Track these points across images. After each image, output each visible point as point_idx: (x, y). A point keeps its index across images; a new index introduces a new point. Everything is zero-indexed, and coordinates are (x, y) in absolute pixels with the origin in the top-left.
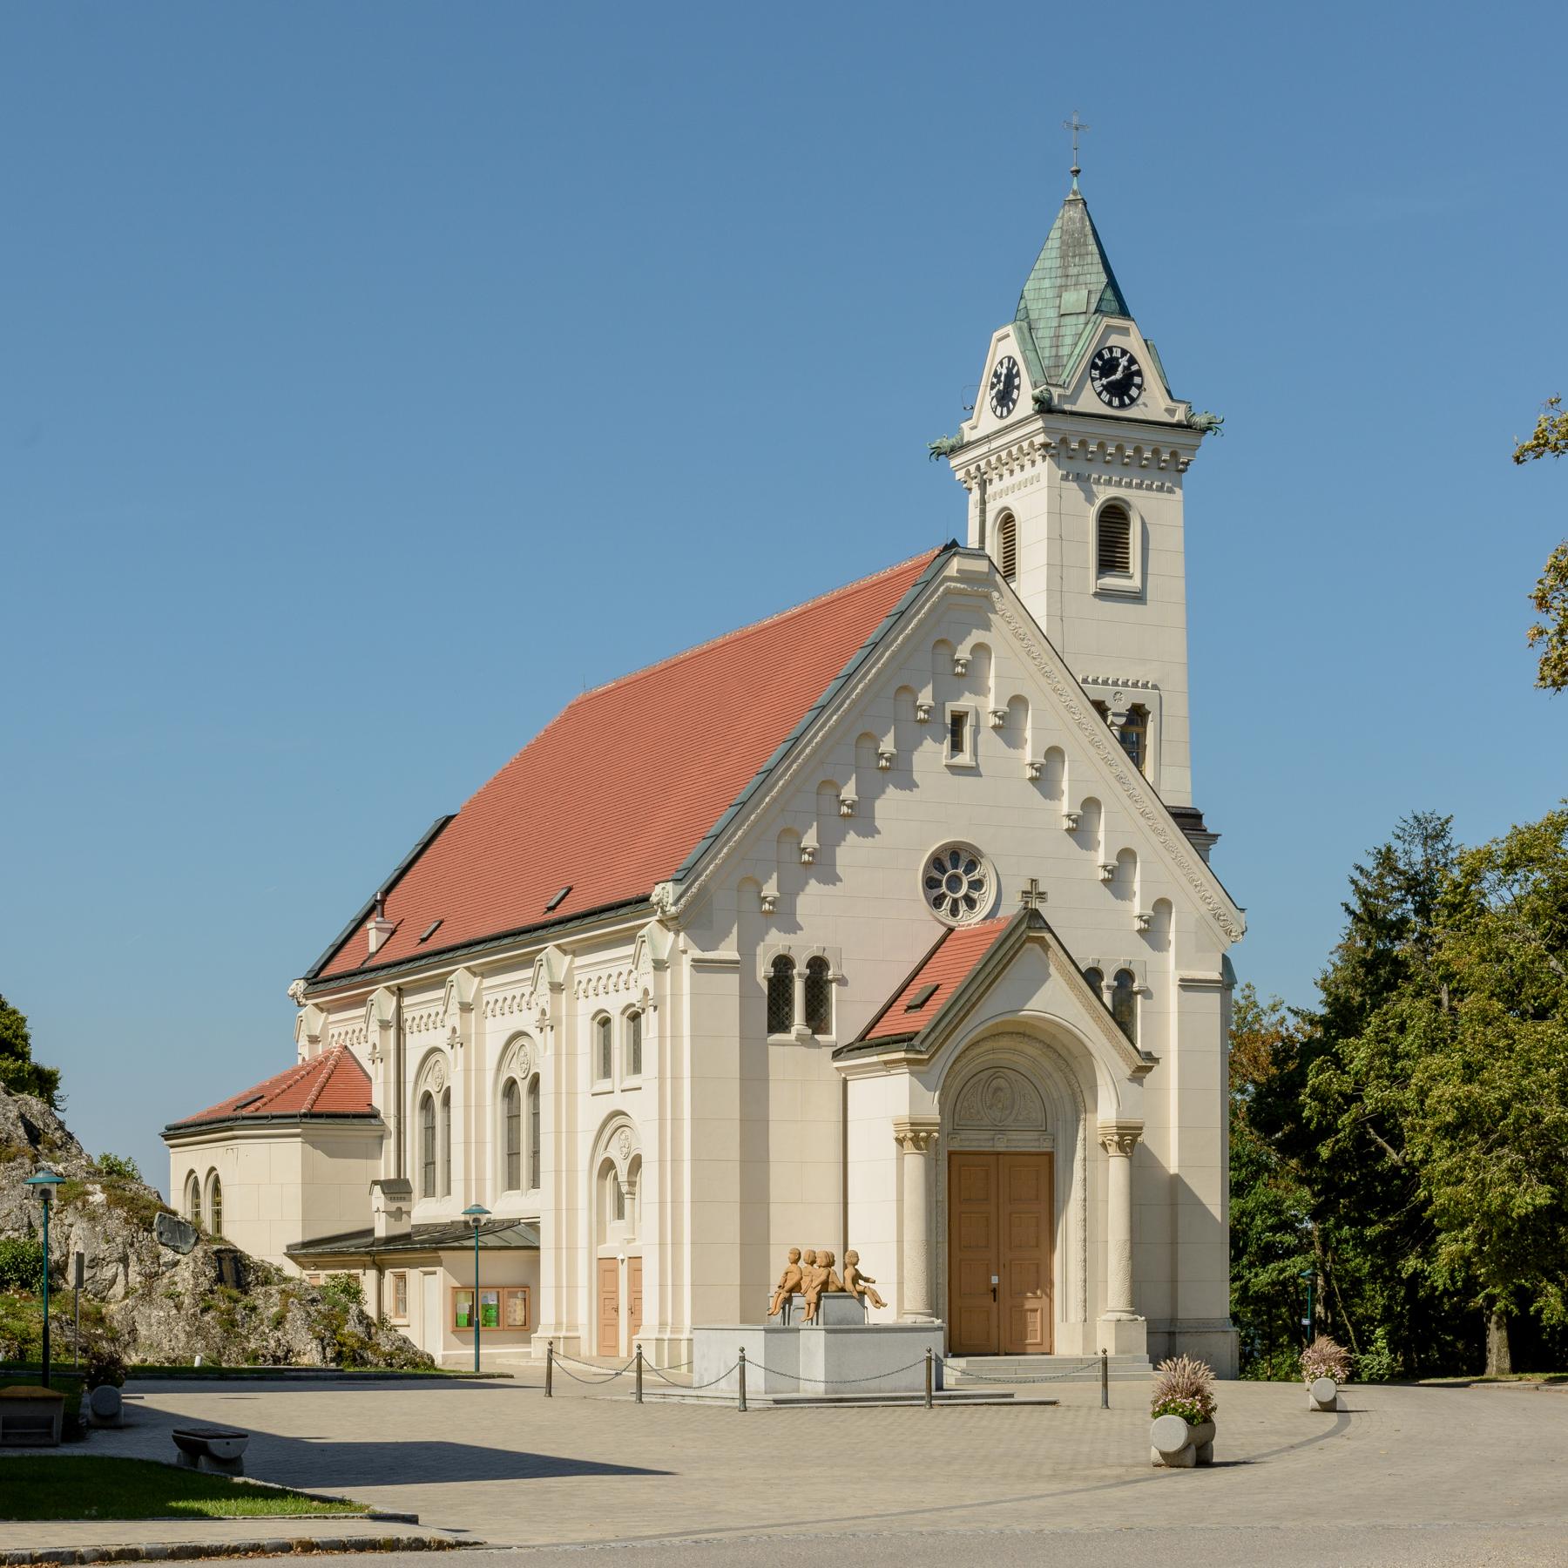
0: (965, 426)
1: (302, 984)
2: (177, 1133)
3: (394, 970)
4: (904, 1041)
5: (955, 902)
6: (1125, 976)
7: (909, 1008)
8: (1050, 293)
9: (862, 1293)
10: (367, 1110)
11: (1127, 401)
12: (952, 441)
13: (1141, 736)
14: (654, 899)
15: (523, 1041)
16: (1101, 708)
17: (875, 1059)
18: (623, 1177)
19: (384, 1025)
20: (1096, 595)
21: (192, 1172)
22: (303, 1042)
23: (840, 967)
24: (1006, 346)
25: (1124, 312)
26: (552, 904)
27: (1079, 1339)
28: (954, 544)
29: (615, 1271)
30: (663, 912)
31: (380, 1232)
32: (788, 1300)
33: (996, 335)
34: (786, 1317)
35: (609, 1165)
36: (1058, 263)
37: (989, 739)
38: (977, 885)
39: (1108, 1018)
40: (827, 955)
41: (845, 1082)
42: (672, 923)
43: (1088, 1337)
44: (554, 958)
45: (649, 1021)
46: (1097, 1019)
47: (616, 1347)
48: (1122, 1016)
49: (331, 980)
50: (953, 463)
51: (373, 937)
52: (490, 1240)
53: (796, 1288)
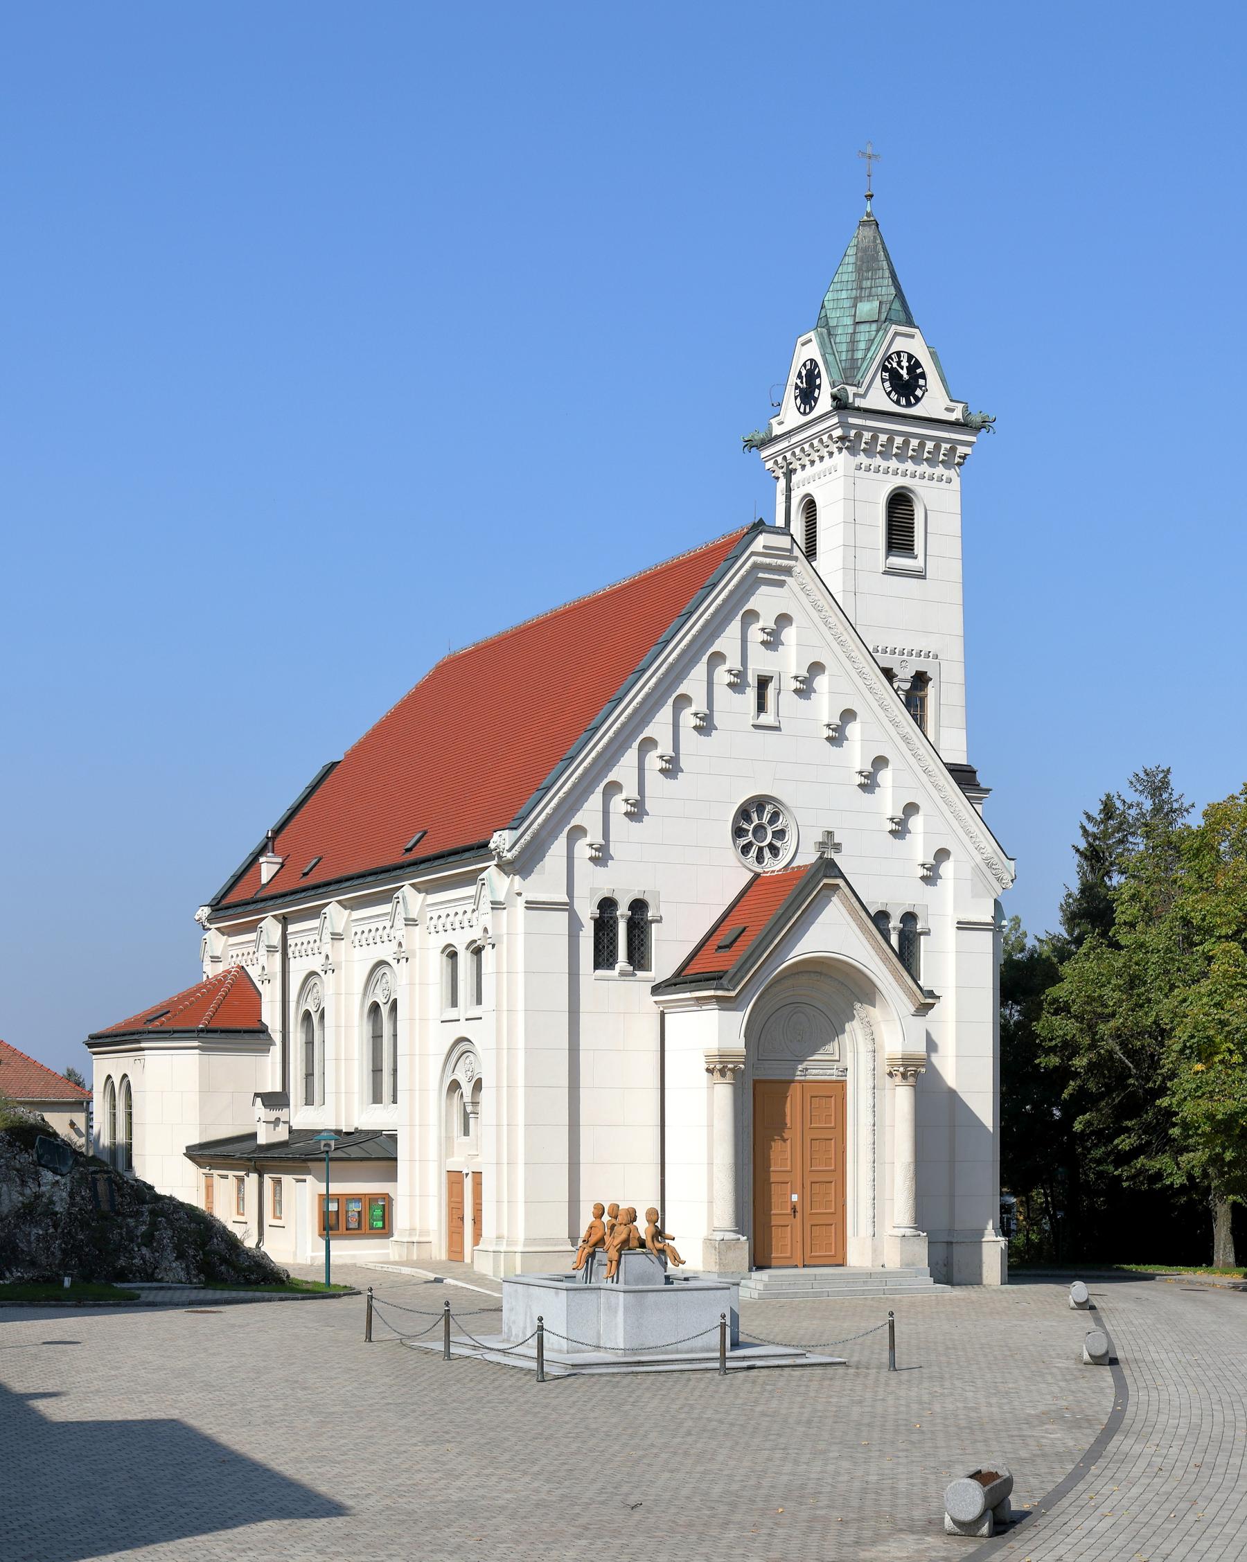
0: (774, 421)
1: (207, 911)
2: (101, 1042)
3: (280, 901)
4: (714, 979)
5: (761, 849)
6: (909, 918)
7: (720, 947)
8: (847, 304)
9: (662, 1251)
10: (257, 1026)
11: (913, 401)
12: (762, 435)
13: (923, 700)
14: (492, 846)
15: (386, 970)
16: (889, 674)
17: (688, 995)
18: (467, 1099)
19: (271, 949)
20: (885, 573)
21: (109, 1077)
22: (207, 960)
23: (658, 908)
24: (809, 350)
25: (909, 322)
26: (409, 846)
27: (869, 1251)
28: (761, 522)
29: (461, 1183)
30: (500, 857)
31: (261, 1140)
32: (592, 1255)
33: (801, 340)
34: (589, 1273)
35: (455, 1086)
36: (853, 277)
37: (788, 698)
38: (780, 834)
39: (895, 960)
40: (647, 898)
41: (663, 1014)
42: (507, 867)
43: (876, 1251)
44: (410, 897)
45: (487, 954)
46: (886, 960)
47: (462, 1252)
48: (906, 955)
49: (236, 905)
50: (764, 454)
51: (267, 869)
52: (355, 1152)
53: (601, 1242)
